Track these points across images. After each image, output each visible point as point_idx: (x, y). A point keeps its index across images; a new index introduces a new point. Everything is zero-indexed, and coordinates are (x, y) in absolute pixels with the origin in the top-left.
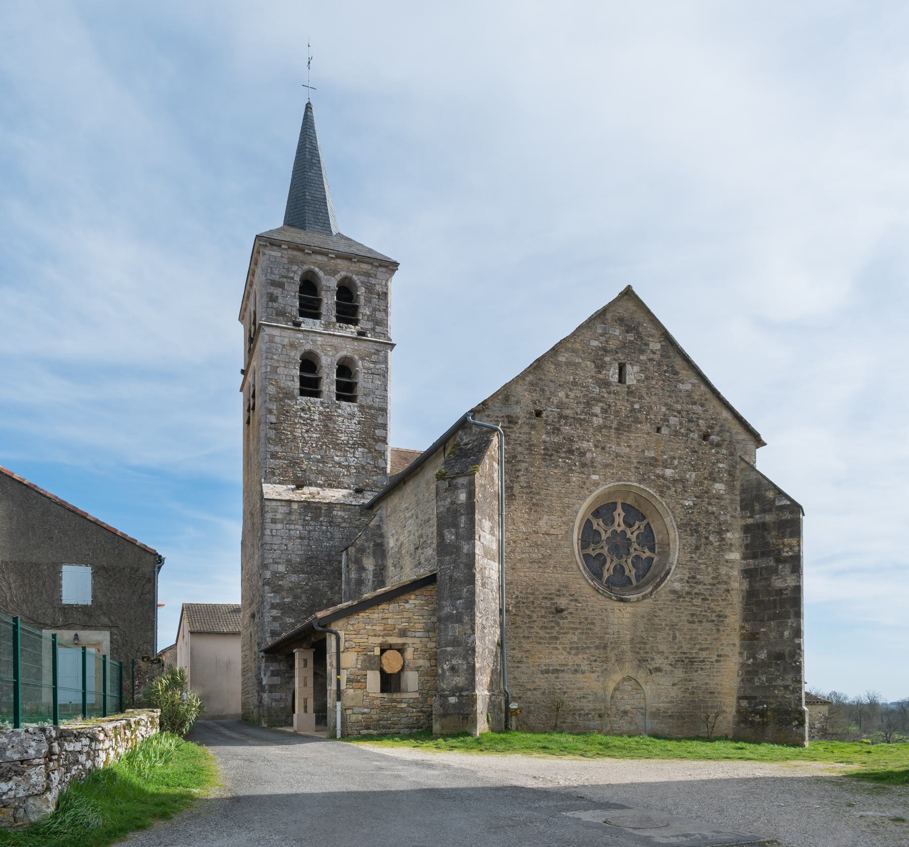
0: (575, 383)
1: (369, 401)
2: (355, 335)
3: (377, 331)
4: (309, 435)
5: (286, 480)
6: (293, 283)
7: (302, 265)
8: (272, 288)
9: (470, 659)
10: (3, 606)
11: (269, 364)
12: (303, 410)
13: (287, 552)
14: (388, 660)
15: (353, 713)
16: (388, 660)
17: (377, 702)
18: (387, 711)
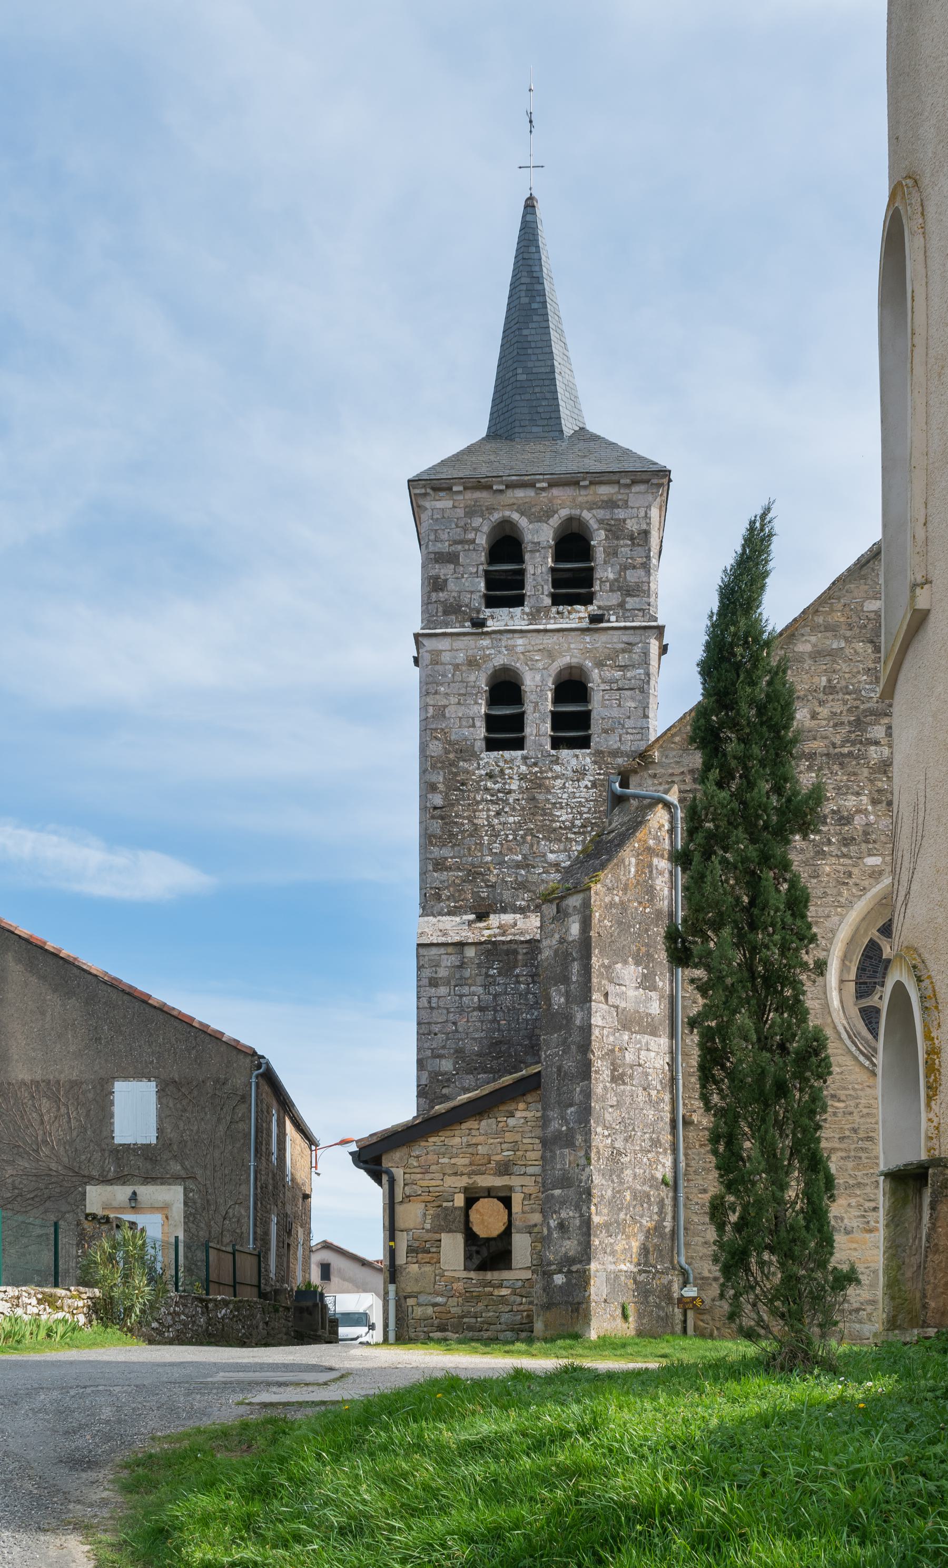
0: (830, 689)
1: (613, 742)
2: (585, 624)
3: (628, 606)
4: (502, 819)
5: (461, 907)
6: (474, 550)
7: (490, 514)
8: (437, 566)
9: (584, 1208)
10: (33, 1150)
11: (432, 702)
12: (490, 776)
13: (458, 1036)
14: (481, 1214)
15: (419, 1305)
16: (481, 1214)
17: (459, 1286)
18: (475, 1301)
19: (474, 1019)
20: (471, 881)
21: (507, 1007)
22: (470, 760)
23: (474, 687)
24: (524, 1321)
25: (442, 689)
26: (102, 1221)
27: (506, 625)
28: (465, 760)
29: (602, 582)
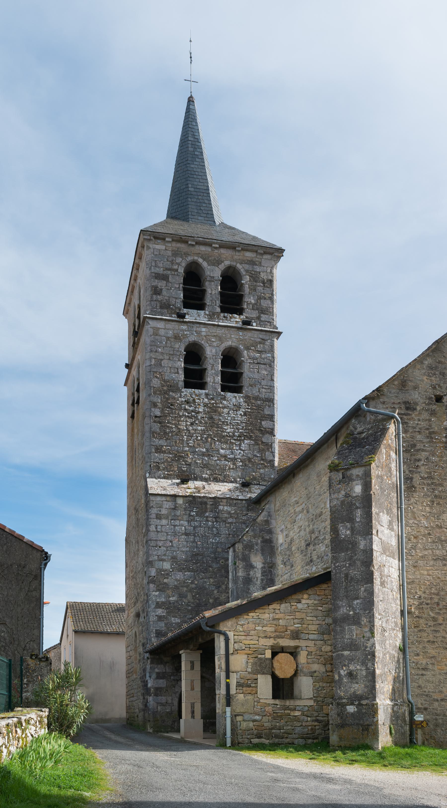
1: (255, 392)
2: (240, 325)
3: (262, 319)
4: (194, 427)
5: (171, 475)
6: (177, 275)
7: (186, 257)
8: (156, 281)
9: (370, 664)
11: (153, 356)
12: (187, 402)
15: (244, 720)
16: (280, 663)
18: (279, 719)
19: (182, 540)
20: (177, 460)
21: (202, 534)
22: (176, 392)
23: (178, 351)
24: (309, 733)
25: (160, 350)
26: (43, 660)
27: (196, 319)
28: (173, 392)
29: (248, 304)
